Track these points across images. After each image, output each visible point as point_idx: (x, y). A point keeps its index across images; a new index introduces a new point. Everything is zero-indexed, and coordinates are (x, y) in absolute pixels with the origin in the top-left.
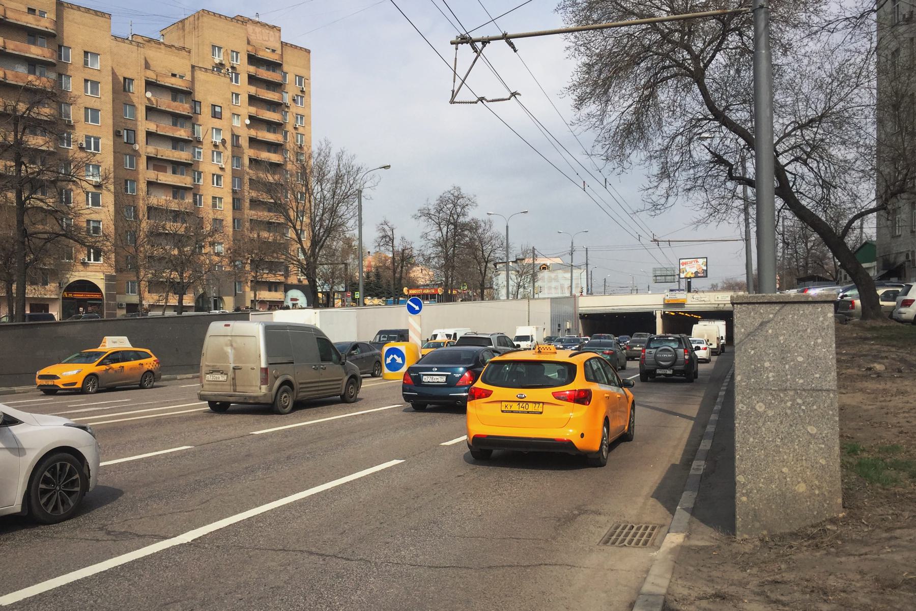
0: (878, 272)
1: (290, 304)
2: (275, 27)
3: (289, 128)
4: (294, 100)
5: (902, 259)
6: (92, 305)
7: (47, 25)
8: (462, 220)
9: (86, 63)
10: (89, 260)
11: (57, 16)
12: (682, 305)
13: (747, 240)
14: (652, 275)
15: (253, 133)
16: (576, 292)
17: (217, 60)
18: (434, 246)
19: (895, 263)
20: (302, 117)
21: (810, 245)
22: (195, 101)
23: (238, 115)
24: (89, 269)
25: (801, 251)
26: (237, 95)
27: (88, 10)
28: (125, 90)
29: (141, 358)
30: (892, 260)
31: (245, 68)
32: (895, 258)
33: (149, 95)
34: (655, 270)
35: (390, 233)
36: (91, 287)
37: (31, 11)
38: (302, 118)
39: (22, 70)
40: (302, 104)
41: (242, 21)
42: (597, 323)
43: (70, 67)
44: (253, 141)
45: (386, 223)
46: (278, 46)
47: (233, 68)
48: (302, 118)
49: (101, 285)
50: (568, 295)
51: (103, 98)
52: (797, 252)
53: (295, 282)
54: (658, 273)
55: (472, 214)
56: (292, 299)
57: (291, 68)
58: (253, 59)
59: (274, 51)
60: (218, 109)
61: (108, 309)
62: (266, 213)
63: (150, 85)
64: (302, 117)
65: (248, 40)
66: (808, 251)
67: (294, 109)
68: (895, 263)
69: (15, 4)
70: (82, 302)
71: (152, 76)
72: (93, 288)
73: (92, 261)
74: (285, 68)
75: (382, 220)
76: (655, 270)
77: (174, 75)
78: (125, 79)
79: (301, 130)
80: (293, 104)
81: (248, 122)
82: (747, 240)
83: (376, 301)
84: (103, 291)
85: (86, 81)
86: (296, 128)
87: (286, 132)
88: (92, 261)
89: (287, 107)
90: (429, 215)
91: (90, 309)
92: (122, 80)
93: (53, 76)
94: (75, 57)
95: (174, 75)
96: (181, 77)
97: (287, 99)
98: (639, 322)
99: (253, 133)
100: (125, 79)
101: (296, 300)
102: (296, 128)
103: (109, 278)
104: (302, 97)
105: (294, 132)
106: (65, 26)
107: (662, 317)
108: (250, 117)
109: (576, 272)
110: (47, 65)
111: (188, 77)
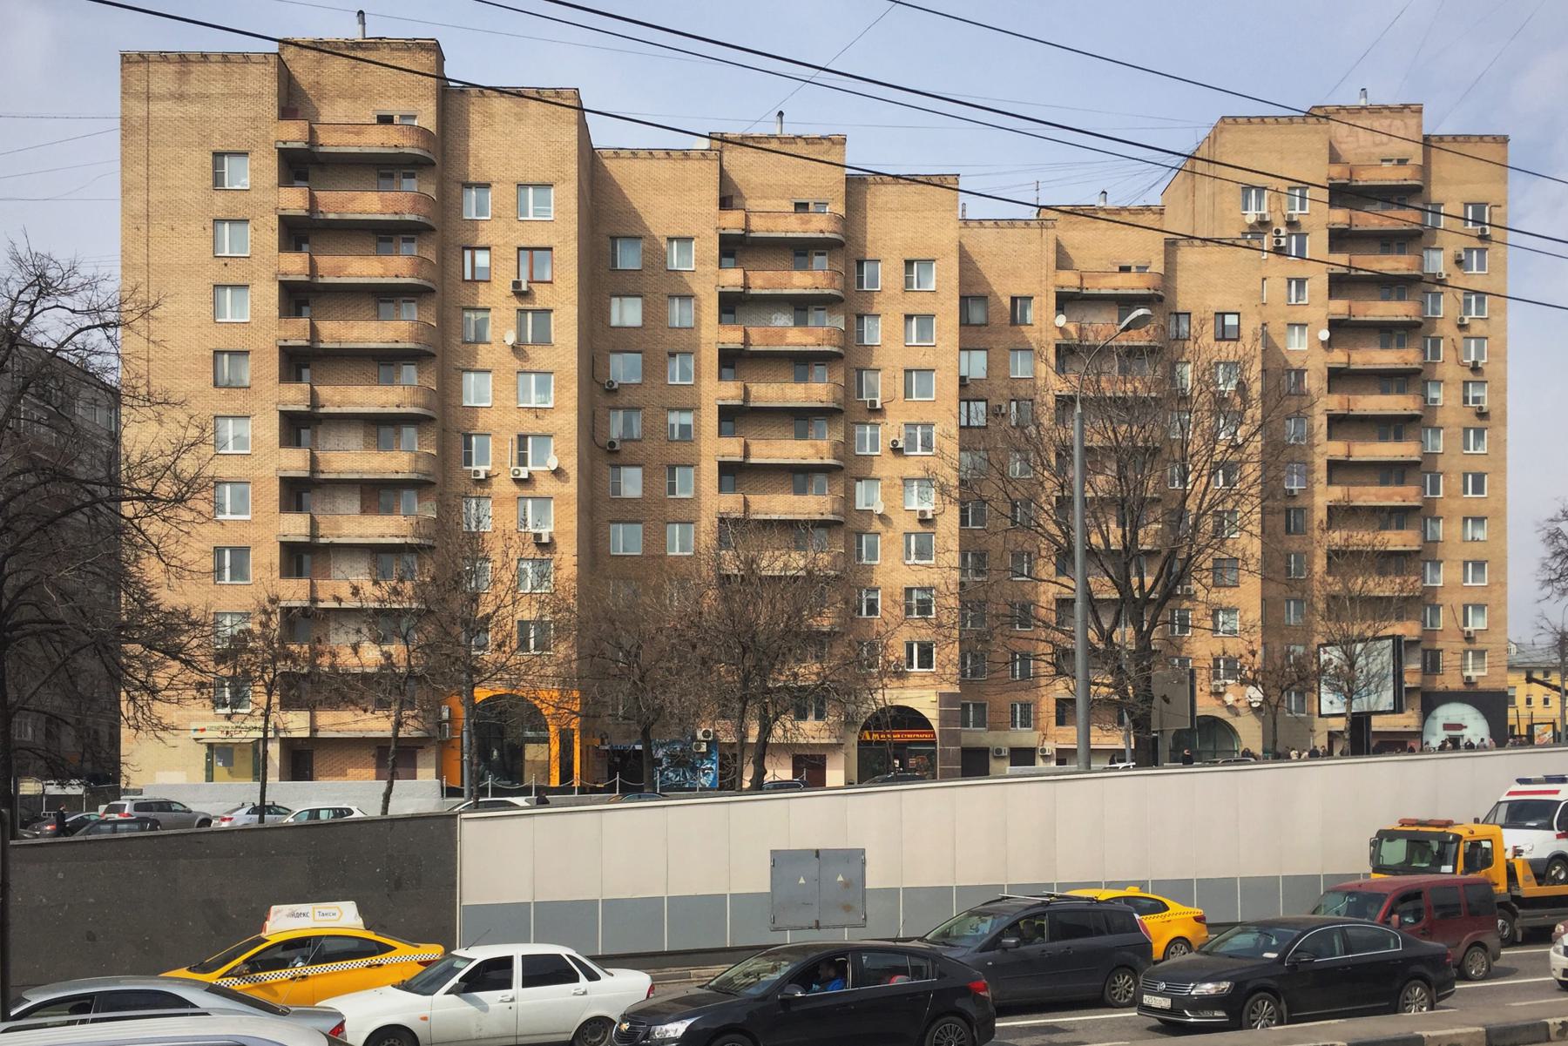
2: (1406, 106)
3: (1446, 329)
4: (1459, 262)
6: (918, 753)
7: (823, 226)
9: (908, 283)
10: (910, 665)
11: (849, 206)
17: (1251, 217)
18: (486, 481)
22: (1177, 314)
23: (1303, 325)
24: (912, 681)
26: (1301, 283)
27: (912, 179)
28: (1014, 322)
29: (372, 954)
31: (1319, 217)
33: (1061, 320)
36: (910, 718)
37: (801, 207)
38: (1480, 301)
39: (782, 320)
40: (1481, 266)
41: (1319, 115)
43: (878, 299)
46: (1415, 154)
47: (1291, 224)
48: (1480, 301)
49: (931, 713)
51: (941, 345)
56: (1447, 727)
57: (1453, 188)
58: (1341, 194)
59: (1402, 162)
60: (1231, 320)
61: (944, 762)
63: (1065, 301)
65: (1331, 147)
69: (773, 202)
70: (901, 750)
71: (1069, 280)
72: (922, 722)
73: (916, 668)
74: (1437, 193)
77: (1125, 269)
78: (1014, 299)
79: (1477, 328)
81: (1324, 335)
84: (935, 725)
85: (909, 317)
86: (1462, 327)
87: (1436, 342)
88: (916, 668)
91: (912, 761)
92: (1007, 302)
93: (839, 322)
94: (886, 276)
95: (1125, 269)
96: (1142, 269)
97: (1438, 262)
99: (1338, 357)
100: (1014, 299)
101: (1460, 727)
102: (1462, 327)
103: (945, 699)
104: (1482, 251)
106: (869, 220)
108: (1334, 325)
109: (154, 88)
110: (824, 302)
111: (1158, 266)
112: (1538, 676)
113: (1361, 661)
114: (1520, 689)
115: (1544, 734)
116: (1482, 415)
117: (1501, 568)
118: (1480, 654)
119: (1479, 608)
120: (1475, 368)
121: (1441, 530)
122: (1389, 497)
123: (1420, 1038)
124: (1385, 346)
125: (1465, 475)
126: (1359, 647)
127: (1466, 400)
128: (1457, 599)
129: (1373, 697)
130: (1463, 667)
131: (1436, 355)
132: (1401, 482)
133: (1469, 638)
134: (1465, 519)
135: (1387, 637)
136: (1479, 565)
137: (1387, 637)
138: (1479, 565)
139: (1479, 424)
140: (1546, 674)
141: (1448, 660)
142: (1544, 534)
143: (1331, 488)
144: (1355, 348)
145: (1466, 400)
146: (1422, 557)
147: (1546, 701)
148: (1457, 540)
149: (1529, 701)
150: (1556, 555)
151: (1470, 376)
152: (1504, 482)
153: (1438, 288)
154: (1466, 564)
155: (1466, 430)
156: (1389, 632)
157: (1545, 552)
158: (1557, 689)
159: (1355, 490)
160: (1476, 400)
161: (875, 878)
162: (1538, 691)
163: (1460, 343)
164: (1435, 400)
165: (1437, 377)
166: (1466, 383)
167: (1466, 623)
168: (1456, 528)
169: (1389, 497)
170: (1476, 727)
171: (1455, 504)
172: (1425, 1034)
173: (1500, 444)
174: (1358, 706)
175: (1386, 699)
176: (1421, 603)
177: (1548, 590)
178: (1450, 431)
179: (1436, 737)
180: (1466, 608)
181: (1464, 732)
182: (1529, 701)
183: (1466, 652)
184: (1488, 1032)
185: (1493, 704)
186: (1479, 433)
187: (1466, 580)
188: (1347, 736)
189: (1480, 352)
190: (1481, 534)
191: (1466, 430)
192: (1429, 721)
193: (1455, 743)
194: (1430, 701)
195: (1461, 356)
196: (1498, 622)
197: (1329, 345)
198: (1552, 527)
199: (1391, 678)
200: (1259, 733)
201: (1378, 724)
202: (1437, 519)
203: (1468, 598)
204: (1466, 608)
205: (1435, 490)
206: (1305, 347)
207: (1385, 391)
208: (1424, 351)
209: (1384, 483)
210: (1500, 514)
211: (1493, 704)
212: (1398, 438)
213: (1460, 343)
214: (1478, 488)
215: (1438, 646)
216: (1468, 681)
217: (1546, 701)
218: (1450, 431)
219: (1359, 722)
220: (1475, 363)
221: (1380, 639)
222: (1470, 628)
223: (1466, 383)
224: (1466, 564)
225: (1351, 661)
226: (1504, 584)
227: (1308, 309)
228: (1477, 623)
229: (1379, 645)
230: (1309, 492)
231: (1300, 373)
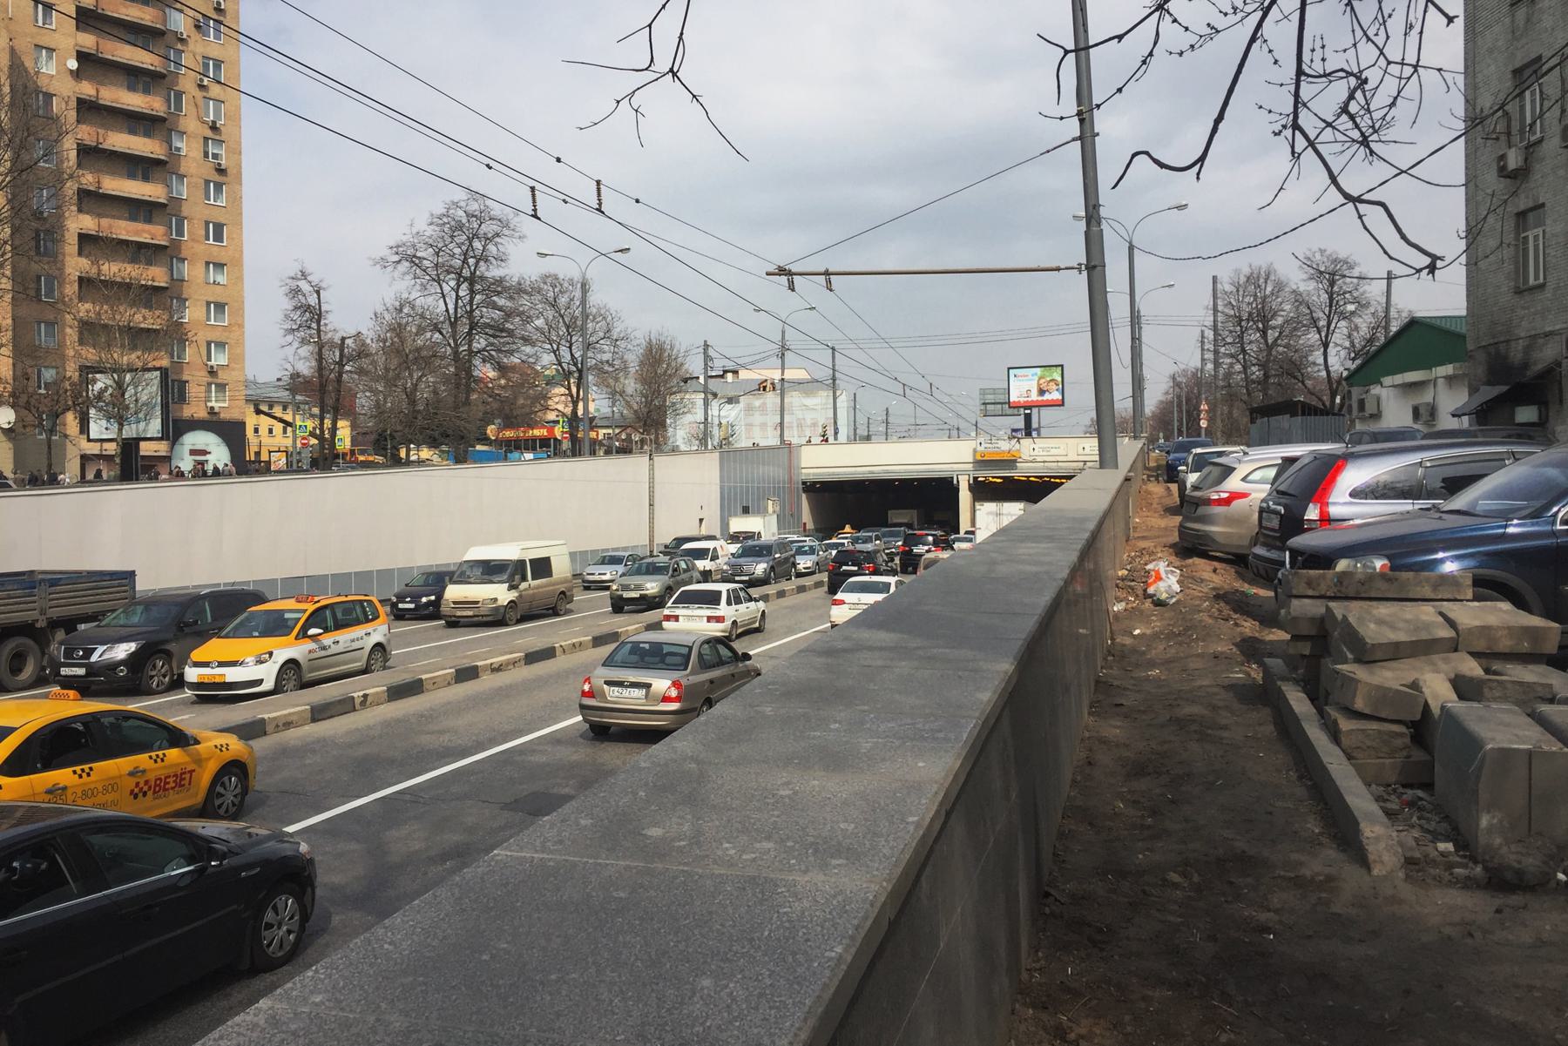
0: (1473, 391)
1: (186, 464)
3: (187, 83)
4: (197, 27)
5: (1548, 353)
8: (494, 272)
12: (1011, 463)
13: (1135, 319)
14: (978, 402)
15: (87, 89)
16: (792, 436)
19: (1525, 365)
20: (218, 64)
21: (1272, 335)
23: (51, 50)
25: (1252, 349)
30: (1516, 354)
32: (1528, 349)
34: (983, 392)
35: (313, 300)
42: (847, 504)
44: (88, 109)
45: (304, 275)
50: (775, 442)
52: (1244, 351)
53: (201, 414)
54: (990, 398)
55: (520, 260)
56: (193, 452)
62: (129, 267)
64: (218, 64)
66: (1270, 348)
67: (199, 47)
68: (1525, 365)
75: (294, 270)
76: (983, 392)
80: (195, 36)
81: (73, 64)
82: (1135, 319)
83: (425, 453)
86: (201, 87)
87: (179, 95)
89: (182, 40)
90: (415, 261)
98: (931, 501)
99: (87, 89)
101: (205, 453)
102: (201, 87)
105: (199, 94)
107: (971, 488)
108: (82, 56)
112: (264, 408)
113: (130, 391)
114: (251, 420)
115: (280, 461)
116: (221, 171)
117: (239, 311)
118: (221, 387)
119: (221, 345)
120: (214, 128)
121: (186, 269)
122: (137, 233)
123: (263, 720)
124: (132, 88)
125: (207, 223)
126: (128, 377)
127: (206, 155)
128: (202, 336)
129: (142, 425)
130: (208, 399)
131: (179, 107)
132: (149, 221)
133: (212, 372)
134: (208, 264)
135: (156, 369)
136: (220, 307)
137: (156, 369)
138: (220, 307)
139: (218, 178)
140: (271, 407)
141: (194, 390)
142: (286, 289)
143: (81, 216)
144: (102, 84)
145: (206, 155)
146: (168, 293)
147: (271, 431)
148: (201, 279)
149: (256, 430)
150: (296, 308)
151: (209, 133)
152: (241, 234)
153: (179, 46)
154: (208, 304)
155: (207, 182)
156: (157, 364)
157: (288, 304)
158: (281, 420)
159: (105, 222)
160: (215, 156)
161: (143, 585)
162: (265, 422)
163: (201, 102)
164: (178, 149)
165: (181, 128)
166: (206, 139)
167: (209, 359)
168: (201, 267)
169: (137, 233)
170: (219, 455)
171: (199, 248)
172: (266, 716)
173: (236, 200)
174: (130, 431)
175: (155, 427)
176: (175, 335)
177: (290, 338)
178: (194, 180)
179: (186, 464)
180: (209, 344)
181: (208, 457)
182: (256, 430)
183: (209, 384)
184: (313, 709)
185: (232, 433)
186: (219, 187)
187: (208, 319)
188: (118, 460)
189: (217, 112)
190: (221, 279)
191: (207, 182)
192: (177, 447)
193: (200, 472)
194: (175, 429)
195: (202, 113)
196: (237, 359)
197: (77, 75)
198: (294, 284)
199: (158, 408)
200: (10, 455)
201: (146, 449)
202: (183, 260)
203: (212, 336)
204: (209, 344)
205: (180, 232)
206: (56, 73)
207: (132, 132)
208: (169, 101)
209: (133, 218)
210: (238, 262)
211: (232, 433)
212: (146, 179)
213: (201, 102)
214: (218, 237)
215: (185, 378)
216: (212, 411)
217: (271, 431)
218: (194, 180)
219: (129, 447)
220: (214, 122)
221: (149, 370)
222: (213, 363)
223: (206, 139)
224: (208, 304)
225: (120, 387)
226: (241, 326)
227: (57, 35)
228: (219, 359)
229: (148, 375)
230: (60, 217)
231: (49, 96)
